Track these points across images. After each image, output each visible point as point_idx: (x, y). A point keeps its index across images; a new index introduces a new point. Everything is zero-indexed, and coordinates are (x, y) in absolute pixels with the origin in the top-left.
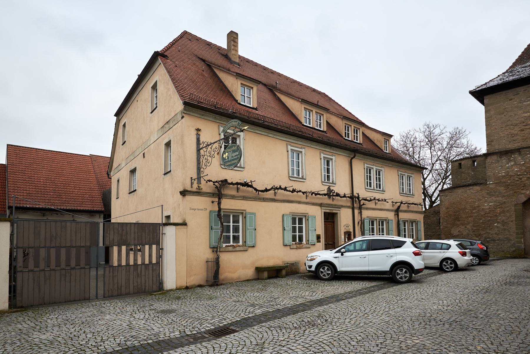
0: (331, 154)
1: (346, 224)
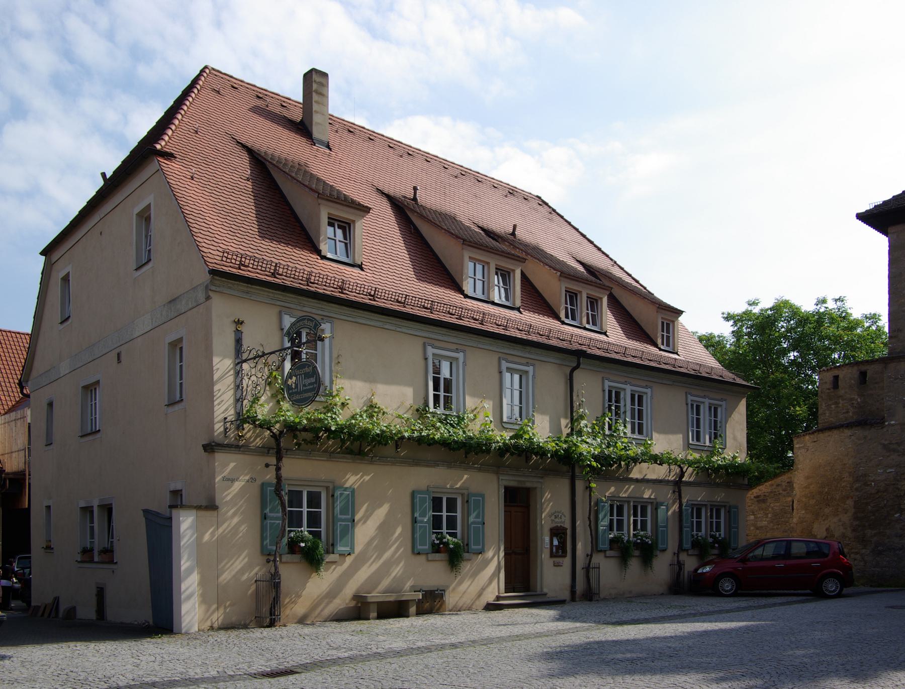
0: (524, 361)
1: (556, 512)
